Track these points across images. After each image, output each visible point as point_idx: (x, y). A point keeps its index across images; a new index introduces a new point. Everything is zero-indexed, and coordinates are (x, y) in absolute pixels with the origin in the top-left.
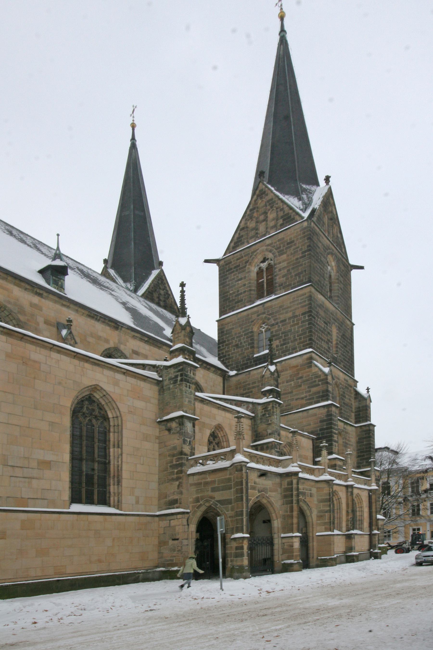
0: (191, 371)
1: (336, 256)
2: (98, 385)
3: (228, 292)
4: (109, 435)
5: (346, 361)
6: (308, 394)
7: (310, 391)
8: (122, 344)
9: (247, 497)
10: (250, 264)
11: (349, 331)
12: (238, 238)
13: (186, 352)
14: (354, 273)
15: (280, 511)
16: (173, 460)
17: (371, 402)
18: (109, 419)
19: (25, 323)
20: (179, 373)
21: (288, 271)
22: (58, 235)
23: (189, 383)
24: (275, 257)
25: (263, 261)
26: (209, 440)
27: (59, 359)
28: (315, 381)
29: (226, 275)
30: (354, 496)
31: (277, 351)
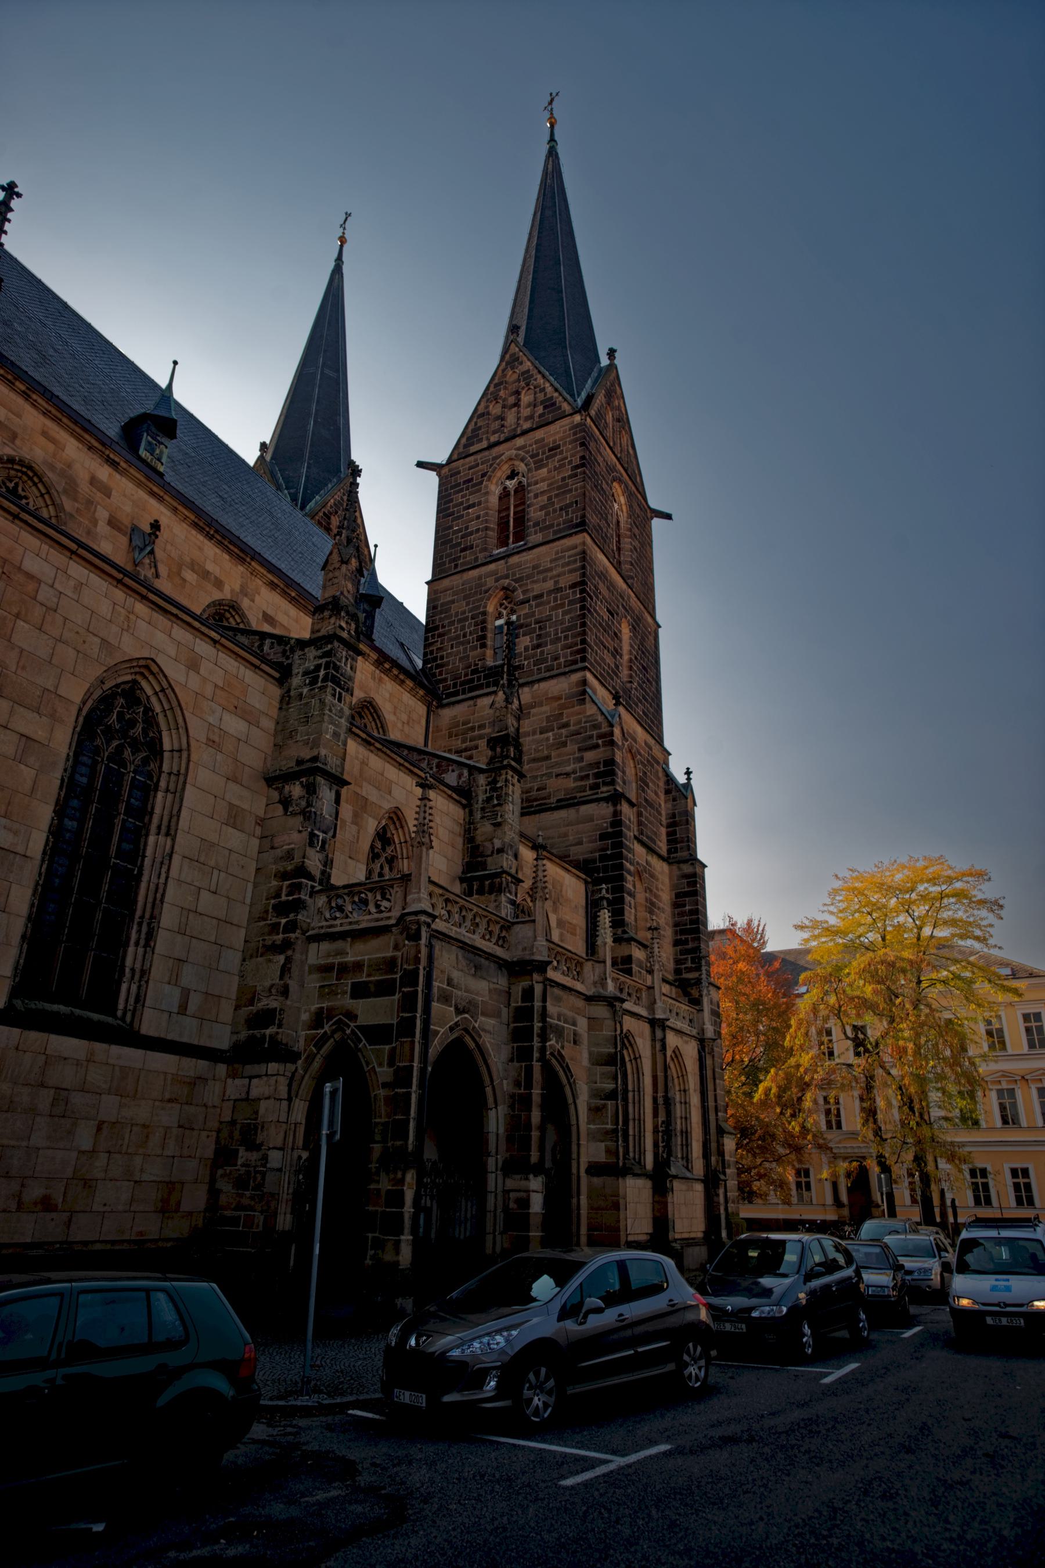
0: (347, 659)
1: (626, 486)
2: (153, 660)
3: (451, 527)
4: (155, 797)
5: (646, 700)
6: (578, 765)
7: (581, 759)
8: (246, 595)
9: (426, 1023)
10: (489, 480)
11: (651, 638)
12: (473, 431)
13: (343, 614)
14: (656, 523)
15: (505, 1082)
16: (281, 888)
17: (695, 804)
18: (161, 752)
19: (71, 516)
20: (324, 661)
21: (550, 498)
22: (175, 363)
23: (340, 687)
24: (529, 470)
25: (510, 477)
26: (372, 847)
27: (84, 582)
28: (591, 737)
29: (450, 495)
30: (669, 1053)
31: (525, 659)
